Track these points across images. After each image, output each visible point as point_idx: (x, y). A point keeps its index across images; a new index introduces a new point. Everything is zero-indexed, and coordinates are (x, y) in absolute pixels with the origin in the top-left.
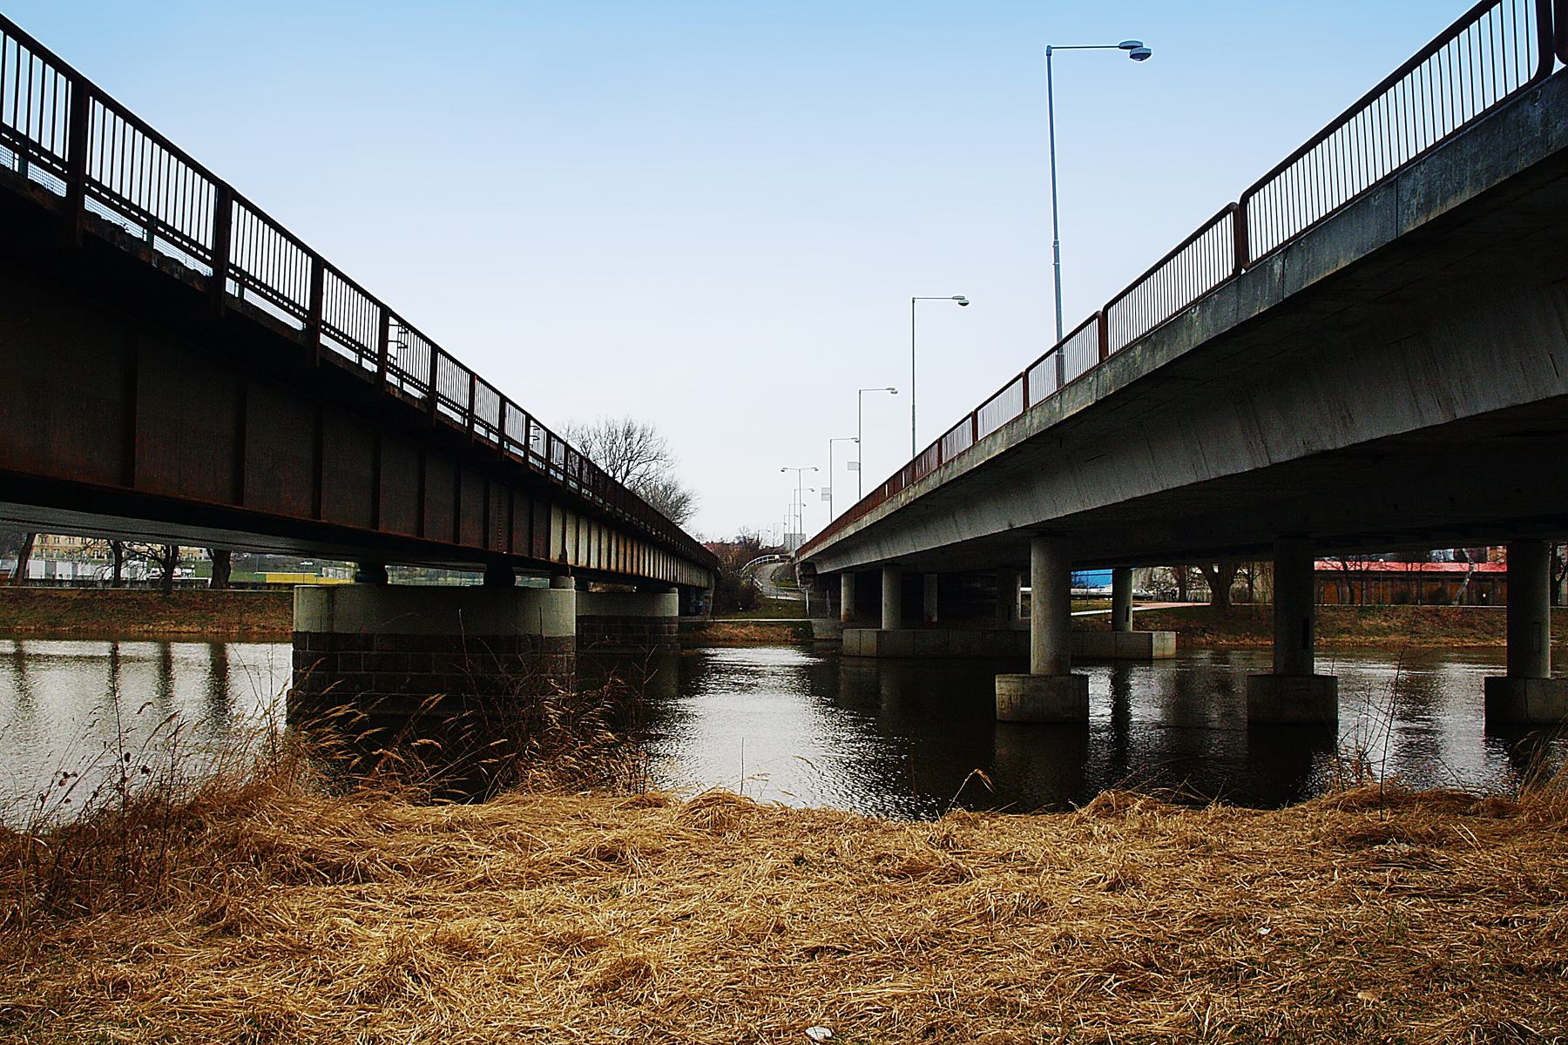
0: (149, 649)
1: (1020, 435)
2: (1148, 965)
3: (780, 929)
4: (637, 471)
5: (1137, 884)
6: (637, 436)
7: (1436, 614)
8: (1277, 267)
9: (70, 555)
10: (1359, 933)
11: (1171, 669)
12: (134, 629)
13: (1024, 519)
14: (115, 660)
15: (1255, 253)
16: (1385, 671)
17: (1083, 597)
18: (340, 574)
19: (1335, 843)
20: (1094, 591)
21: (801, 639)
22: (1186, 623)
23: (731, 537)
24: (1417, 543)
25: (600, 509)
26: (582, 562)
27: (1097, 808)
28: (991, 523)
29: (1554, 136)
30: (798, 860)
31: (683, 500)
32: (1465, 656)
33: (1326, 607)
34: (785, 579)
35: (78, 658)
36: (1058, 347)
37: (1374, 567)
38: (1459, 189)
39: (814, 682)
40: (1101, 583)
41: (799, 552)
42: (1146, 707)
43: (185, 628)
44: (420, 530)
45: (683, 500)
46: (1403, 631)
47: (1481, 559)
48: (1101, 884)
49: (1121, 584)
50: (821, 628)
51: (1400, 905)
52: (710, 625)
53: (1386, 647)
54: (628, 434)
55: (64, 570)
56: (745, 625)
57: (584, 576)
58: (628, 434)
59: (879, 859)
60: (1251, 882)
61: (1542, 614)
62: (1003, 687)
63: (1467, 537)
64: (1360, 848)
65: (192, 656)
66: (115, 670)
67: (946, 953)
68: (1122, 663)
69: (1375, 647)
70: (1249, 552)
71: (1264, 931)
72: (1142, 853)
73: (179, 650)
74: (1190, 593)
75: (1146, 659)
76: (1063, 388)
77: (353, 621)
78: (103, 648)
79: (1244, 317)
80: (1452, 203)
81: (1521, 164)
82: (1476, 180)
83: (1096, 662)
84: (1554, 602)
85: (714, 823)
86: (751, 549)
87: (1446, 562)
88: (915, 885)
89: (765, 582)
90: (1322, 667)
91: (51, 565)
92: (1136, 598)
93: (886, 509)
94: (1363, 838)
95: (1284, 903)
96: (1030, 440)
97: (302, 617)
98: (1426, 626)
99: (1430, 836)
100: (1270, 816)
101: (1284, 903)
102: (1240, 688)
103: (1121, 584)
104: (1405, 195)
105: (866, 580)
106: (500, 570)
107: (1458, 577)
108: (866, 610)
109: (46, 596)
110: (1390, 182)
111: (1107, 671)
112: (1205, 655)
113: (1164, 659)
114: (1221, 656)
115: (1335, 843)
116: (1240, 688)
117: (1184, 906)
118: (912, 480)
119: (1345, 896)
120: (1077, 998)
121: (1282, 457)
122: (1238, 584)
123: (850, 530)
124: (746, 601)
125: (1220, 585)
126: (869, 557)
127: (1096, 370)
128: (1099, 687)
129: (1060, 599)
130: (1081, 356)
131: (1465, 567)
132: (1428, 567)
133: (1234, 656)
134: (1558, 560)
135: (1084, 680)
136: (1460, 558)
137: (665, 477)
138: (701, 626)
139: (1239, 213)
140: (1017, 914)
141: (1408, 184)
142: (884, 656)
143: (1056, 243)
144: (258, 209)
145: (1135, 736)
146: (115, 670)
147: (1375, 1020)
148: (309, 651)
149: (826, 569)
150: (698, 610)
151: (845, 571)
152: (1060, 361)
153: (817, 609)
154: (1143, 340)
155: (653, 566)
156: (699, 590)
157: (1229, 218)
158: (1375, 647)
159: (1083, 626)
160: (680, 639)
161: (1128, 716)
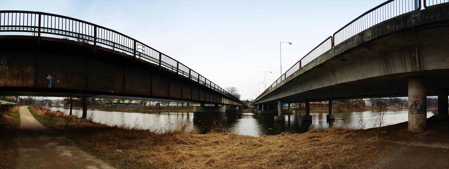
0: (181, 113)
1: (276, 88)
2: (282, 160)
3: (234, 155)
4: (234, 92)
5: (283, 146)
6: (234, 88)
7: (322, 108)
8: (304, 68)
9: (173, 103)
10: (309, 152)
11: (295, 115)
12: (179, 111)
13: (277, 98)
14: (178, 115)
15: (302, 66)
16: (318, 114)
17: (284, 107)
18: (199, 105)
19: (308, 138)
20: (286, 106)
21: (253, 112)
22: (296, 110)
23: (245, 100)
24: (320, 100)
25: (228, 97)
26: (226, 103)
27: (281, 134)
28: (273, 98)
29: (333, 55)
30: (241, 143)
31: (240, 96)
32: (325, 112)
33: (311, 107)
34: (251, 105)
35: (174, 114)
36: (281, 77)
37: (316, 103)
38: (323, 60)
39: (255, 117)
40: (287, 105)
41: (253, 102)
42: (292, 118)
43: (184, 111)
44: (205, 100)
45: (240, 96)
46: (319, 110)
47: (327, 102)
48: (279, 147)
49: (289, 105)
50: (255, 110)
51: (314, 147)
52: (242, 110)
53: (317, 112)
54: (233, 88)
55: (173, 105)
56: (246, 110)
57: (227, 105)
58: (233, 88)
59: (251, 143)
60: (298, 145)
61: (332, 108)
62: (275, 117)
63: (325, 100)
64: (311, 139)
65: (185, 114)
66: (178, 116)
67: (256, 159)
68: (289, 114)
69: (316, 112)
70: (303, 101)
71: (298, 153)
72: (286, 141)
73: (184, 113)
74: (297, 106)
75: (292, 114)
76: (282, 82)
77: (200, 110)
78: (176, 113)
79: (300, 74)
80: (322, 62)
81: (329, 58)
82: (325, 59)
83: (286, 114)
84: (333, 106)
85: (232, 138)
86: (247, 101)
87: (323, 103)
88: (255, 147)
89: (249, 105)
90: (311, 114)
91: (172, 104)
92: (291, 107)
93: (262, 97)
94: (311, 137)
95: (301, 148)
96: (277, 89)
97: (194, 110)
98: (321, 109)
99: (319, 136)
100: (302, 134)
101: (301, 148)
102: (302, 116)
103: (289, 105)
104: (318, 61)
105: (260, 105)
106: (216, 104)
107: (324, 104)
108: (260, 108)
109: (171, 108)
110: (316, 59)
111: (288, 115)
112: (299, 113)
113: (294, 114)
114: (300, 113)
115: (308, 138)
116: (302, 116)
117: (289, 150)
118: (265, 93)
119: (309, 147)
120: (271, 166)
121: (305, 91)
122: (302, 105)
123: (258, 99)
124: (246, 107)
125: (300, 105)
126: (260, 102)
127: (284, 80)
128: (287, 118)
129: (282, 107)
130: (283, 78)
131: (325, 103)
132: (322, 103)
133: (302, 113)
134: (333, 102)
135: (284, 116)
136: (325, 102)
137: (238, 93)
138: (241, 110)
139: (300, 62)
140: (266, 152)
141: (318, 59)
142: (262, 114)
143: (281, 65)
144: (57, 39)
145: (291, 123)
146: (178, 116)
147: (310, 166)
148: (196, 114)
149: (256, 104)
150: (241, 109)
151: (263, 103)
152: (281, 79)
153: (255, 108)
154: (290, 76)
155: (235, 103)
156: (241, 106)
157: (299, 62)
158: (316, 112)
159: (285, 110)
160: (239, 112)
161: (290, 120)
